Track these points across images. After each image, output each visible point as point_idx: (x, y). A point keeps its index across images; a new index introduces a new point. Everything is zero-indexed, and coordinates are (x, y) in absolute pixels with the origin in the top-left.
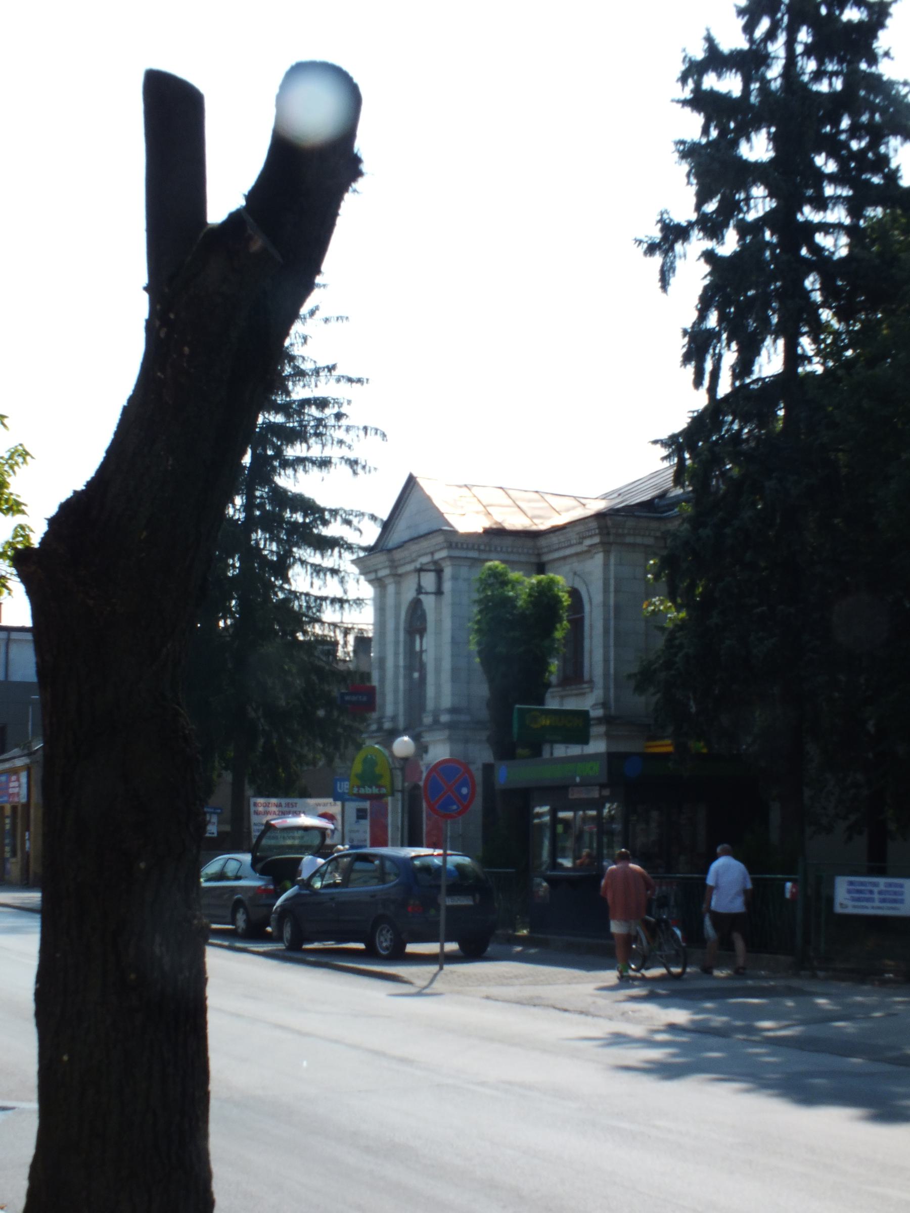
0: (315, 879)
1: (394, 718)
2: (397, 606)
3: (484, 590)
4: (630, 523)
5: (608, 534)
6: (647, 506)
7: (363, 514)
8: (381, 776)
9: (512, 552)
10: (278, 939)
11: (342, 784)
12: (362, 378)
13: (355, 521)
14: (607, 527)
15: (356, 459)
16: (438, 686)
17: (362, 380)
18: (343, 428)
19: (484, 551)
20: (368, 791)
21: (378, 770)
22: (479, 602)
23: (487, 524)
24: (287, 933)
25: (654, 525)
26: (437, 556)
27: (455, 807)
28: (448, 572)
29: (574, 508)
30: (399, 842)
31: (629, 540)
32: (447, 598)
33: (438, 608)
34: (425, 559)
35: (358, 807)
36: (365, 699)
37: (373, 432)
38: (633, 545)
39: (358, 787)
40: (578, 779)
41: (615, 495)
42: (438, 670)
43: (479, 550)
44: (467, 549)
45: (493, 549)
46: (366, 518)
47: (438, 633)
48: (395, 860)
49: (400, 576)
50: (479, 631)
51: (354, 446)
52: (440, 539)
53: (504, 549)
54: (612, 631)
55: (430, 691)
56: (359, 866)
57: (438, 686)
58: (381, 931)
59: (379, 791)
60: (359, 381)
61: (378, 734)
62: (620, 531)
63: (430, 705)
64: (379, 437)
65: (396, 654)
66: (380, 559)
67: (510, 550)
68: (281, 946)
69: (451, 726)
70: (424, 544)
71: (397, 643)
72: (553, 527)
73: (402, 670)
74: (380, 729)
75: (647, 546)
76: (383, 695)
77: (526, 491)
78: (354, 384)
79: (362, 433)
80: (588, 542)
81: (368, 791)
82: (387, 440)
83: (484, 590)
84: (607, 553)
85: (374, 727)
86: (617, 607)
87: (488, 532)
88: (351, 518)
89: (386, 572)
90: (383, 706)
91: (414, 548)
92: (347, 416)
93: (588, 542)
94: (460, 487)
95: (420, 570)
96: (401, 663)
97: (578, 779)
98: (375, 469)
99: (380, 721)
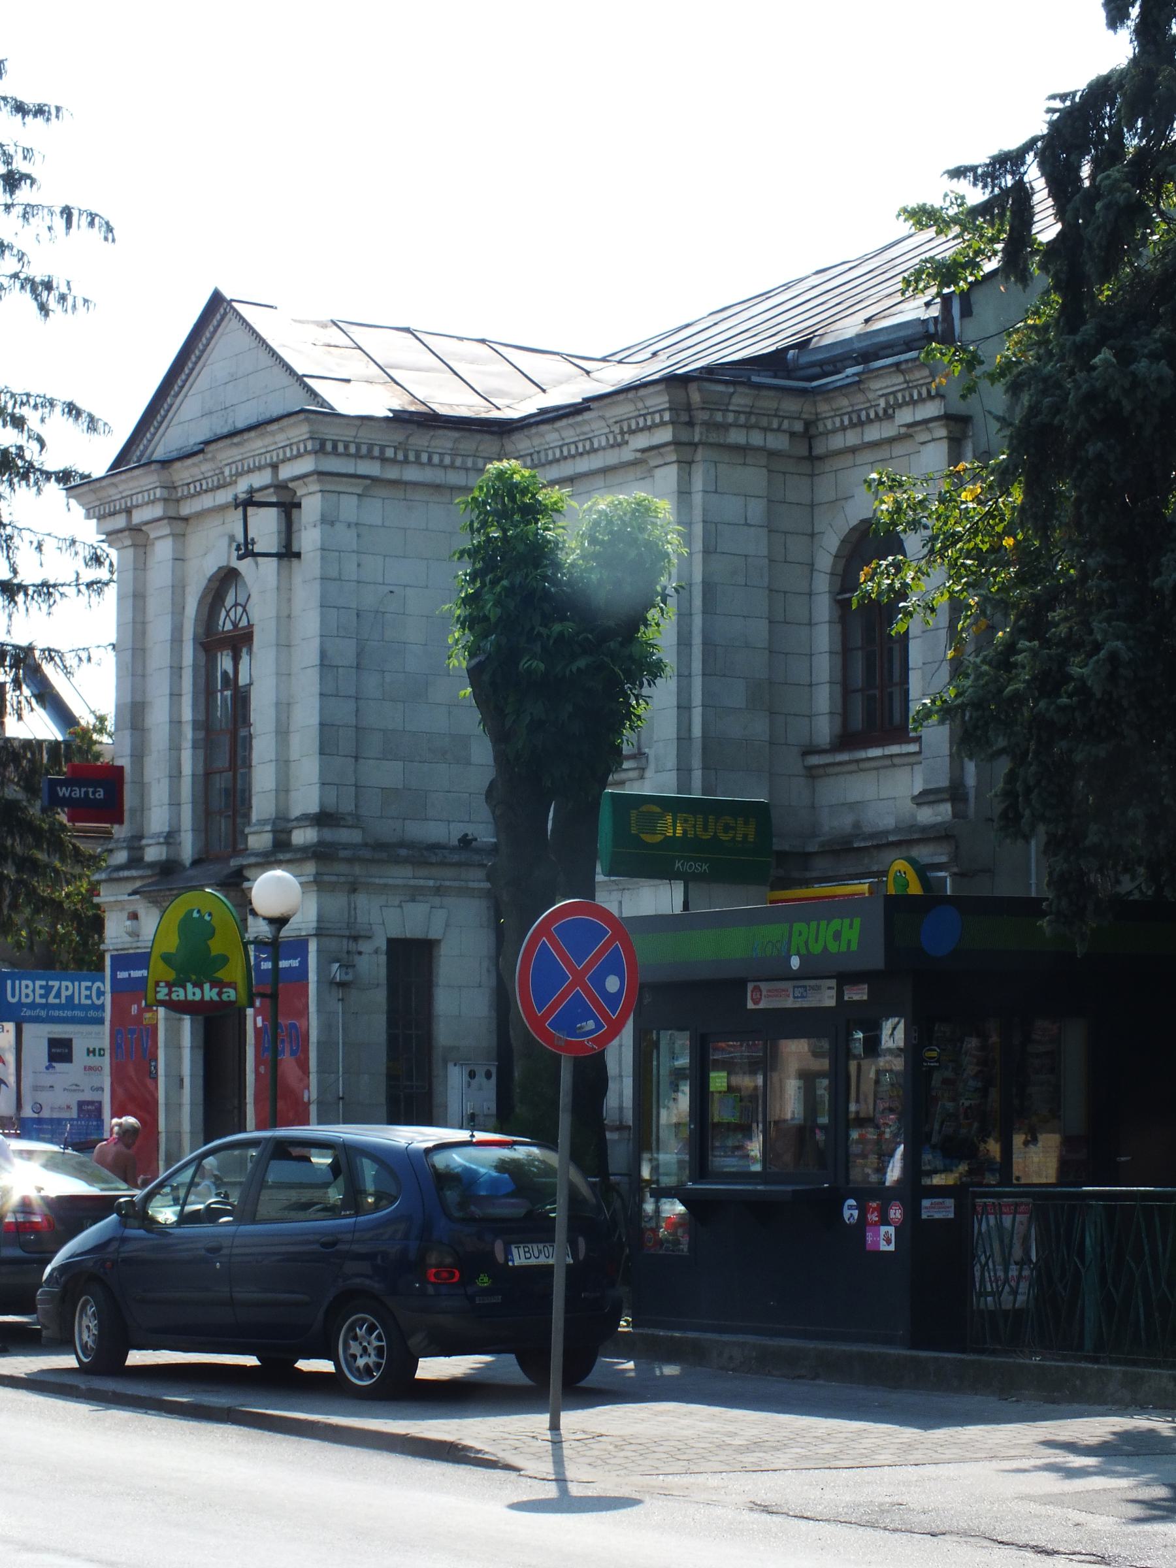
0: (157, 1201)
1: (170, 838)
2: (178, 588)
3: (484, 524)
4: (741, 399)
5: (690, 424)
6: (773, 362)
7: (52, 403)
8: (224, 960)
9: (452, 466)
10: (63, 1344)
11: (17, 982)
12: (45, 105)
13: (32, 417)
14: (689, 408)
15: (46, 279)
16: (283, 764)
17: (46, 108)
18: (17, 211)
19: (394, 461)
20: (194, 994)
21: (216, 947)
22: (473, 553)
23: (399, 402)
24: (87, 1329)
25: (791, 405)
26: (285, 472)
27: (591, 1024)
28: (312, 505)
29: (568, 379)
30: (383, 1111)
31: (736, 437)
32: (310, 563)
33: (284, 590)
34: (261, 479)
35: (51, 1036)
36: (100, 794)
37: (84, 220)
38: (742, 450)
39: (169, 985)
40: (795, 962)
41: (647, 354)
42: (283, 733)
43: (383, 460)
44: (358, 456)
45: (412, 458)
46: (58, 410)
47: (284, 645)
48: (384, 1157)
49: (186, 519)
50: (468, 623)
51: (31, 255)
52: (299, 432)
53: (436, 459)
54: (697, 640)
55: (263, 779)
56: (279, 1171)
57: (283, 764)
58: (352, 1328)
59: (220, 994)
60: (40, 111)
61: (134, 873)
62: (719, 417)
63: (262, 806)
64: (97, 234)
65: (175, 695)
66: (147, 481)
67: (447, 460)
68: (68, 1361)
69: (320, 853)
70: (256, 444)
71: (176, 670)
72: (543, 411)
73: (188, 732)
74: (135, 861)
75: (772, 454)
76: (141, 786)
77: (461, 339)
78: (29, 119)
79: (59, 223)
80: (642, 441)
81: (194, 994)
82: (113, 240)
83: (484, 524)
84: (686, 464)
85: (121, 857)
86: (709, 588)
87: (400, 418)
88: (25, 411)
89: (157, 511)
90: (141, 809)
91: (227, 454)
92: (33, 181)
93: (642, 441)
94: (324, 326)
95: (248, 502)
96: (187, 714)
97: (795, 962)
98: (86, 301)
99: (135, 843)
